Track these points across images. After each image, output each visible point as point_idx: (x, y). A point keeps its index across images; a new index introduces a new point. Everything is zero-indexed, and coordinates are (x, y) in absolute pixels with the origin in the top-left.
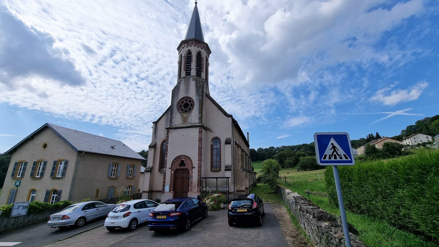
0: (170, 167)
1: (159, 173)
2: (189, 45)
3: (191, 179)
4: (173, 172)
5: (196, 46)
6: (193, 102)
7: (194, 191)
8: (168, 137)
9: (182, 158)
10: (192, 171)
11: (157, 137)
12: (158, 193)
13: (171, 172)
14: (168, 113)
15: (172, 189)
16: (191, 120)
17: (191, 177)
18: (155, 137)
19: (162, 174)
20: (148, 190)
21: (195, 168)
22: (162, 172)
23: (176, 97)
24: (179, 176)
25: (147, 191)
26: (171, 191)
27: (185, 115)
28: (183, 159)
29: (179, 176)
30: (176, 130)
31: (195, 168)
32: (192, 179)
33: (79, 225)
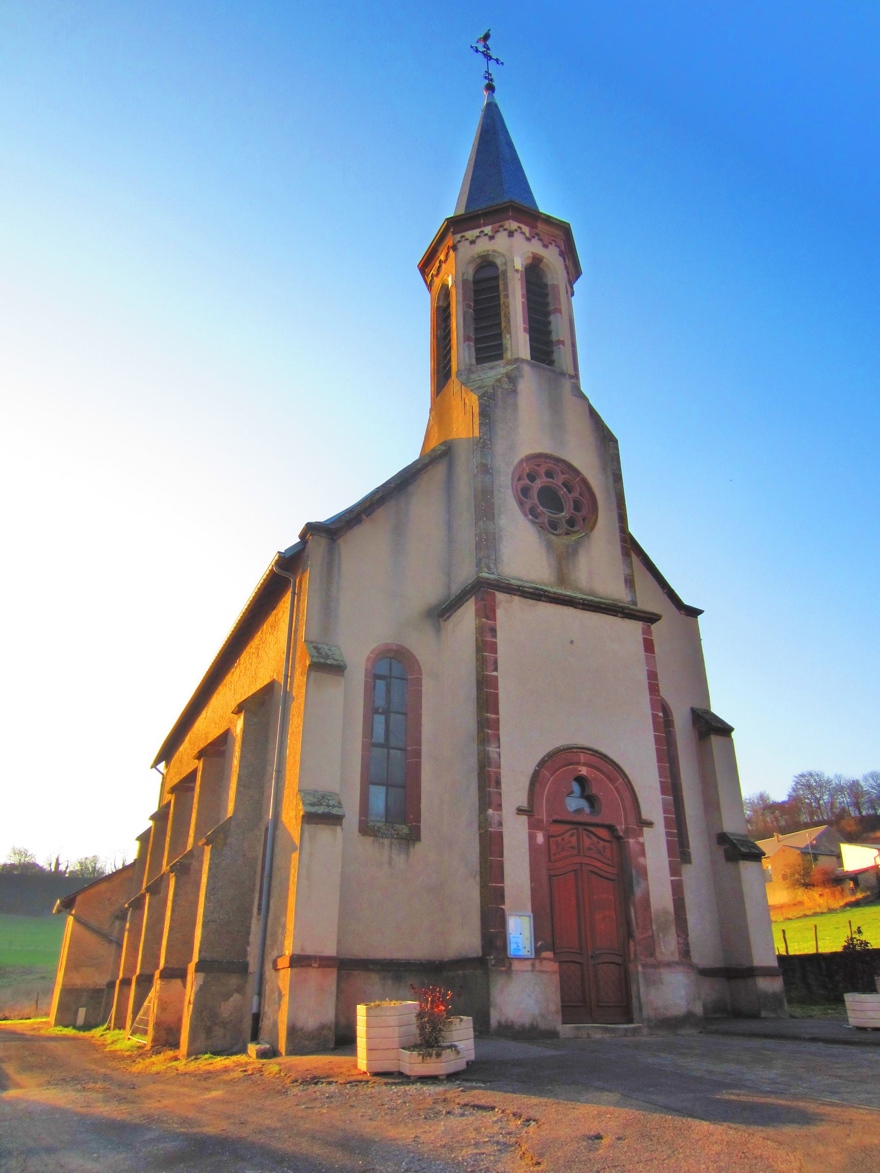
0: (522, 800)
2: (501, 229)
4: (540, 838)
8: (493, 631)
9: (579, 763)
13: (532, 837)
20: (330, 950)
21: (650, 824)
28: (583, 771)
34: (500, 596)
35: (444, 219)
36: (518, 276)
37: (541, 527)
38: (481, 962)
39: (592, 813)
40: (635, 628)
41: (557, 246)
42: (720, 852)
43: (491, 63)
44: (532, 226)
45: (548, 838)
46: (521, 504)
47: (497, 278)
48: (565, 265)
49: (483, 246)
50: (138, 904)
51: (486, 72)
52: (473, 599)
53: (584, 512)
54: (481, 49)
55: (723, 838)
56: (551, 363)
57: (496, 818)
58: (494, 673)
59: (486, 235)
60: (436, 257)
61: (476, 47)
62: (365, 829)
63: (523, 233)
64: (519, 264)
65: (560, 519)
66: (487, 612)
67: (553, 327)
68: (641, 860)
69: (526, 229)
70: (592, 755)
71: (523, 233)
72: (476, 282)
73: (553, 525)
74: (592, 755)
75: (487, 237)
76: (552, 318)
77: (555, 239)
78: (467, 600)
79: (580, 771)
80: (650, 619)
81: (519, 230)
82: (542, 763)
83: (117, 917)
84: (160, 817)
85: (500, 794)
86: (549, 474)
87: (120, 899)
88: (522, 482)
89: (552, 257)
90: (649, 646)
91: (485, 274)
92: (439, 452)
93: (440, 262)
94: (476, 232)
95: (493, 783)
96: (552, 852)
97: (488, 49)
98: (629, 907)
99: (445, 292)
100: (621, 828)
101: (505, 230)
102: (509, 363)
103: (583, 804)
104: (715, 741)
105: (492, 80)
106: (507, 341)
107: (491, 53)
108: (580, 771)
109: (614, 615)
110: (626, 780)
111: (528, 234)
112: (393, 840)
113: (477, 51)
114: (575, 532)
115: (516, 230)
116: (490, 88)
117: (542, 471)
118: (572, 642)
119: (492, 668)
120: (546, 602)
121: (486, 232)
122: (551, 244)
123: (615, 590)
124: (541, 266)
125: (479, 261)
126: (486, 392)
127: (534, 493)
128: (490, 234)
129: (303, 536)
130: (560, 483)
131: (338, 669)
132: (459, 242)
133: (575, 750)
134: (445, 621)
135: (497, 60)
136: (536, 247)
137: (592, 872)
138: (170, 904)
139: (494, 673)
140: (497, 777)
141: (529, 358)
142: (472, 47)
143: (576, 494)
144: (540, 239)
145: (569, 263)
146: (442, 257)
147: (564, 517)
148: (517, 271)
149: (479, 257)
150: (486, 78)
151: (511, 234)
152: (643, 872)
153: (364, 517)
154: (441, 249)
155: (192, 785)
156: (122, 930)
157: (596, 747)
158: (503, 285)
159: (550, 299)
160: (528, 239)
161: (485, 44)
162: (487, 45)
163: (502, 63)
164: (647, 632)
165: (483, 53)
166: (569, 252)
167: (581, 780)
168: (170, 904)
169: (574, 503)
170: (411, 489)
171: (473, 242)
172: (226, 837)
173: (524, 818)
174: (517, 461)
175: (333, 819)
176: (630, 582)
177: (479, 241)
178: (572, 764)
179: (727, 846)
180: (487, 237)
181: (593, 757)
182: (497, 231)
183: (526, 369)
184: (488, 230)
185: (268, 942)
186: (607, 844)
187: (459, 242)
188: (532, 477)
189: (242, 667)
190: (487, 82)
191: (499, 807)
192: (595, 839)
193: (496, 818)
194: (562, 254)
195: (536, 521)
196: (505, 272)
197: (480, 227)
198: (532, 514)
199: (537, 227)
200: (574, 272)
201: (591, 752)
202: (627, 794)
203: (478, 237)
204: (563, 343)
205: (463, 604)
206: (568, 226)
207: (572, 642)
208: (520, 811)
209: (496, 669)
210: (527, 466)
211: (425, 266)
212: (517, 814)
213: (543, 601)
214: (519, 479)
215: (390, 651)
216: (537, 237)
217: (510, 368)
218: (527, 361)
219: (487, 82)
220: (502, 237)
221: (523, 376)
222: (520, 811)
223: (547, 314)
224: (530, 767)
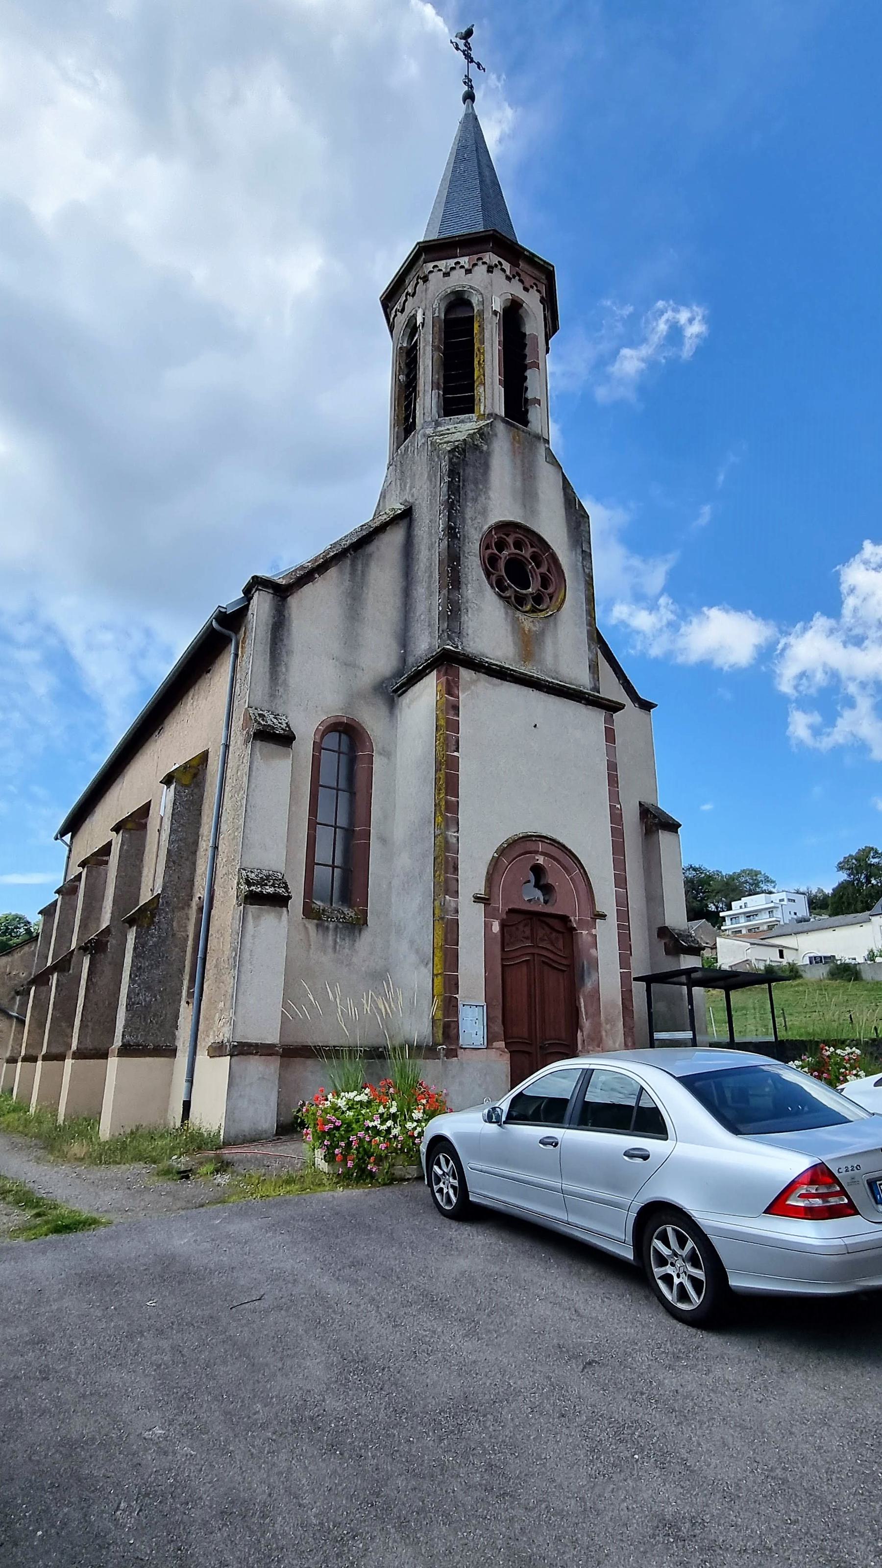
0: (480, 888)
1: (311, 925)
2: (480, 263)
3: (589, 973)
4: (496, 927)
5: (531, 290)
6: (490, 564)
7: (609, 1042)
8: (456, 708)
9: (537, 852)
10: (594, 932)
11: (285, 683)
12: (310, 1062)
13: (487, 926)
14: (359, 567)
15: (498, 1028)
16: (556, 656)
17: (589, 964)
18: (276, 684)
19: (331, 938)
20: (272, 1037)
21: (603, 916)
22: (331, 925)
23: (475, 500)
24: (518, 954)
25: (274, 1046)
26: (495, 1044)
27: (528, 623)
28: (541, 860)
29: (518, 954)
30: (494, 685)
31: (603, 916)
32: (594, 978)
33: (665, 1231)
34: (465, 674)
35: (415, 244)
36: (496, 320)
37: (508, 602)
38: (427, 1051)
39: (546, 902)
40: (596, 718)
41: (538, 291)
42: (661, 945)
43: (473, 66)
44: (514, 264)
45: (503, 926)
46: (488, 575)
47: (471, 320)
48: (545, 315)
49: (458, 280)
50: (41, 979)
51: (466, 76)
52: (435, 672)
53: (551, 590)
54: (462, 47)
55: (663, 932)
56: (526, 423)
57: (453, 905)
58: (456, 754)
59: (462, 267)
60: (403, 288)
61: (457, 44)
62: (309, 912)
63: (503, 270)
64: (498, 305)
65: (526, 595)
66: (451, 688)
67: (528, 383)
68: (593, 951)
69: (506, 266)
70: (550, 844)
71: (503, 270)
72: (446, 321)
73: (520, 601)
74: (550, 844)
75: (463, 270)
76: (528, 373)
77: (537, 283)
78: (427, 674)
79: (538, 860)
80: (612, 707)
81: (499, 267)
82: (502, 851)
83: (18, 993)
84: (68, 890)
85: (458, 881)
86: (518, 545)
87: (21, 974)
88: (489, 551)
89: (532, 303)
90: (610, 735)
91: (460, 314)
92: (400, 512)
93: (408, 294)
94: (451, 262)
95: (452, 870)
96: (506, 941)
97: (470, 49)
98: (579, 998)
99: (412, 329)
100: (574, 921)
101: (484, 263)
102: (481, 417)
103: (538, 894)
104: (664, 837)
105: (472, 87)
106: (479, 391)
107: (473, 54)
108: (538, 860)
109: (578, 702)
110: (582, 871)
111: (508, 273)
112: (339, 924)
113: (457, 48)
114: (541, 611)
115: (496, 266)
116: (469, 97)
117: (510, 540)
118: (535, 726)
119: (454, 748)
120: (511, 682)
121: (462, 263)
122: (532, 287)
123: (581, 678)
124: (521, 311)
125: (452, 298)
126: (457, 447)
127: (502, 564)
128: (467, 266)
129: (248, 592)
130: (528, 556)
131: (286, 739)
132: (431, 272)
133: (534, 839)
134: (400, 696)
135: (479, 65)
136: (516, 289)
137: (544, 962)
138: (83, 982)
139: (456, 754)
140: (455, 863)
141: (503, 414)
142: (452, 42)
143: (544, 569)
144: (521, 281)
145: (548, 315)
146: (410, 290)
147: (531, 594)
148: (495, 313)
149: (452, 292)
150: (465, 83)
151: (490, 269)
152: (594, 964)
153: (317, 576)
154: (411, 276)
155: (105, 858)
156: (24, 1004)
157: (554, 837)
158: (478, 328)
159: (527, 351)
160: (508, 278)
161: (467, 42)
162: (469, 44)
163: (484, 69)
164: (609, 720)
165: (464, 52)
166: (550, 302)
167: (538, 870)
168: (83, 982)
169: (541, 577)
170: (371, 548)
171: (447, 274)
172: (153, 916)
173: (599, 908)
174: (486, 527)
175: (280, 901)
176: (594, 668)
177: (453, 273)
178: (530, 852)
179: (666, 940)
180: (463, 270)
181: (550, 846)
182: (475, 265)
183: (500, 427)
184: (464, 261)
185: (201, 1027)
186: (560, 936)
187: (431, 272)
188: (501, 545)
189: (164, 739)
190: (466, 88)
191: (456, 894)
192: (548, 930)
193: (453, 905)
194: (542, 301)
195: (503, 595)
196: (481, 313)
197: (456, 257)
198: (499, 586)
199: (519, 265)
200: (552, 325)
201: (549, 841)
202: (582, 886)
203: (453, 269)
204: (538, 402)
205: (422, 678)
206: (552, 269)
207: (535, 726)
208: (477, 899)
209: (457, 750)
210: (495, 534)
211: (389, 299)
212: (474, 902)
213: (507, 681)
214: (488, 547)
215: (341, 724)
216: (517, 278)
217: (482, 423)
218: (500, 417)
219: (466, 88)
220: (481, 269)
221: (496, 435)
222: (477, 899)
223: (525, 368)
224: (490, 853)
